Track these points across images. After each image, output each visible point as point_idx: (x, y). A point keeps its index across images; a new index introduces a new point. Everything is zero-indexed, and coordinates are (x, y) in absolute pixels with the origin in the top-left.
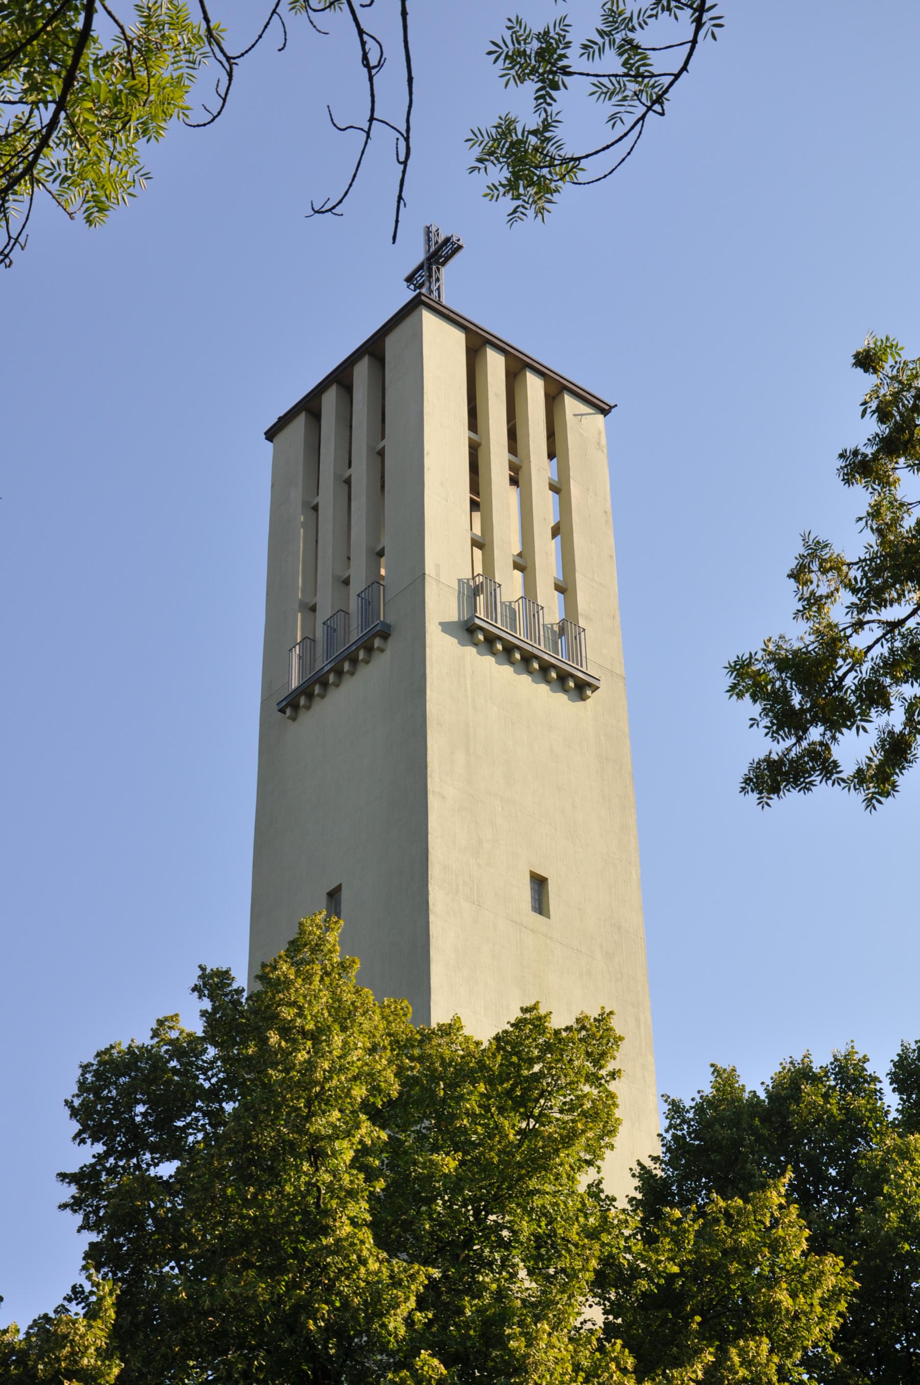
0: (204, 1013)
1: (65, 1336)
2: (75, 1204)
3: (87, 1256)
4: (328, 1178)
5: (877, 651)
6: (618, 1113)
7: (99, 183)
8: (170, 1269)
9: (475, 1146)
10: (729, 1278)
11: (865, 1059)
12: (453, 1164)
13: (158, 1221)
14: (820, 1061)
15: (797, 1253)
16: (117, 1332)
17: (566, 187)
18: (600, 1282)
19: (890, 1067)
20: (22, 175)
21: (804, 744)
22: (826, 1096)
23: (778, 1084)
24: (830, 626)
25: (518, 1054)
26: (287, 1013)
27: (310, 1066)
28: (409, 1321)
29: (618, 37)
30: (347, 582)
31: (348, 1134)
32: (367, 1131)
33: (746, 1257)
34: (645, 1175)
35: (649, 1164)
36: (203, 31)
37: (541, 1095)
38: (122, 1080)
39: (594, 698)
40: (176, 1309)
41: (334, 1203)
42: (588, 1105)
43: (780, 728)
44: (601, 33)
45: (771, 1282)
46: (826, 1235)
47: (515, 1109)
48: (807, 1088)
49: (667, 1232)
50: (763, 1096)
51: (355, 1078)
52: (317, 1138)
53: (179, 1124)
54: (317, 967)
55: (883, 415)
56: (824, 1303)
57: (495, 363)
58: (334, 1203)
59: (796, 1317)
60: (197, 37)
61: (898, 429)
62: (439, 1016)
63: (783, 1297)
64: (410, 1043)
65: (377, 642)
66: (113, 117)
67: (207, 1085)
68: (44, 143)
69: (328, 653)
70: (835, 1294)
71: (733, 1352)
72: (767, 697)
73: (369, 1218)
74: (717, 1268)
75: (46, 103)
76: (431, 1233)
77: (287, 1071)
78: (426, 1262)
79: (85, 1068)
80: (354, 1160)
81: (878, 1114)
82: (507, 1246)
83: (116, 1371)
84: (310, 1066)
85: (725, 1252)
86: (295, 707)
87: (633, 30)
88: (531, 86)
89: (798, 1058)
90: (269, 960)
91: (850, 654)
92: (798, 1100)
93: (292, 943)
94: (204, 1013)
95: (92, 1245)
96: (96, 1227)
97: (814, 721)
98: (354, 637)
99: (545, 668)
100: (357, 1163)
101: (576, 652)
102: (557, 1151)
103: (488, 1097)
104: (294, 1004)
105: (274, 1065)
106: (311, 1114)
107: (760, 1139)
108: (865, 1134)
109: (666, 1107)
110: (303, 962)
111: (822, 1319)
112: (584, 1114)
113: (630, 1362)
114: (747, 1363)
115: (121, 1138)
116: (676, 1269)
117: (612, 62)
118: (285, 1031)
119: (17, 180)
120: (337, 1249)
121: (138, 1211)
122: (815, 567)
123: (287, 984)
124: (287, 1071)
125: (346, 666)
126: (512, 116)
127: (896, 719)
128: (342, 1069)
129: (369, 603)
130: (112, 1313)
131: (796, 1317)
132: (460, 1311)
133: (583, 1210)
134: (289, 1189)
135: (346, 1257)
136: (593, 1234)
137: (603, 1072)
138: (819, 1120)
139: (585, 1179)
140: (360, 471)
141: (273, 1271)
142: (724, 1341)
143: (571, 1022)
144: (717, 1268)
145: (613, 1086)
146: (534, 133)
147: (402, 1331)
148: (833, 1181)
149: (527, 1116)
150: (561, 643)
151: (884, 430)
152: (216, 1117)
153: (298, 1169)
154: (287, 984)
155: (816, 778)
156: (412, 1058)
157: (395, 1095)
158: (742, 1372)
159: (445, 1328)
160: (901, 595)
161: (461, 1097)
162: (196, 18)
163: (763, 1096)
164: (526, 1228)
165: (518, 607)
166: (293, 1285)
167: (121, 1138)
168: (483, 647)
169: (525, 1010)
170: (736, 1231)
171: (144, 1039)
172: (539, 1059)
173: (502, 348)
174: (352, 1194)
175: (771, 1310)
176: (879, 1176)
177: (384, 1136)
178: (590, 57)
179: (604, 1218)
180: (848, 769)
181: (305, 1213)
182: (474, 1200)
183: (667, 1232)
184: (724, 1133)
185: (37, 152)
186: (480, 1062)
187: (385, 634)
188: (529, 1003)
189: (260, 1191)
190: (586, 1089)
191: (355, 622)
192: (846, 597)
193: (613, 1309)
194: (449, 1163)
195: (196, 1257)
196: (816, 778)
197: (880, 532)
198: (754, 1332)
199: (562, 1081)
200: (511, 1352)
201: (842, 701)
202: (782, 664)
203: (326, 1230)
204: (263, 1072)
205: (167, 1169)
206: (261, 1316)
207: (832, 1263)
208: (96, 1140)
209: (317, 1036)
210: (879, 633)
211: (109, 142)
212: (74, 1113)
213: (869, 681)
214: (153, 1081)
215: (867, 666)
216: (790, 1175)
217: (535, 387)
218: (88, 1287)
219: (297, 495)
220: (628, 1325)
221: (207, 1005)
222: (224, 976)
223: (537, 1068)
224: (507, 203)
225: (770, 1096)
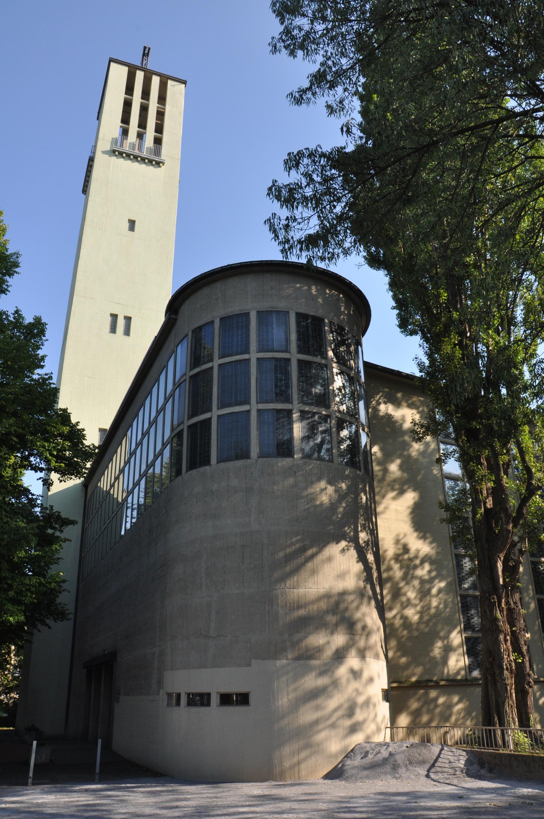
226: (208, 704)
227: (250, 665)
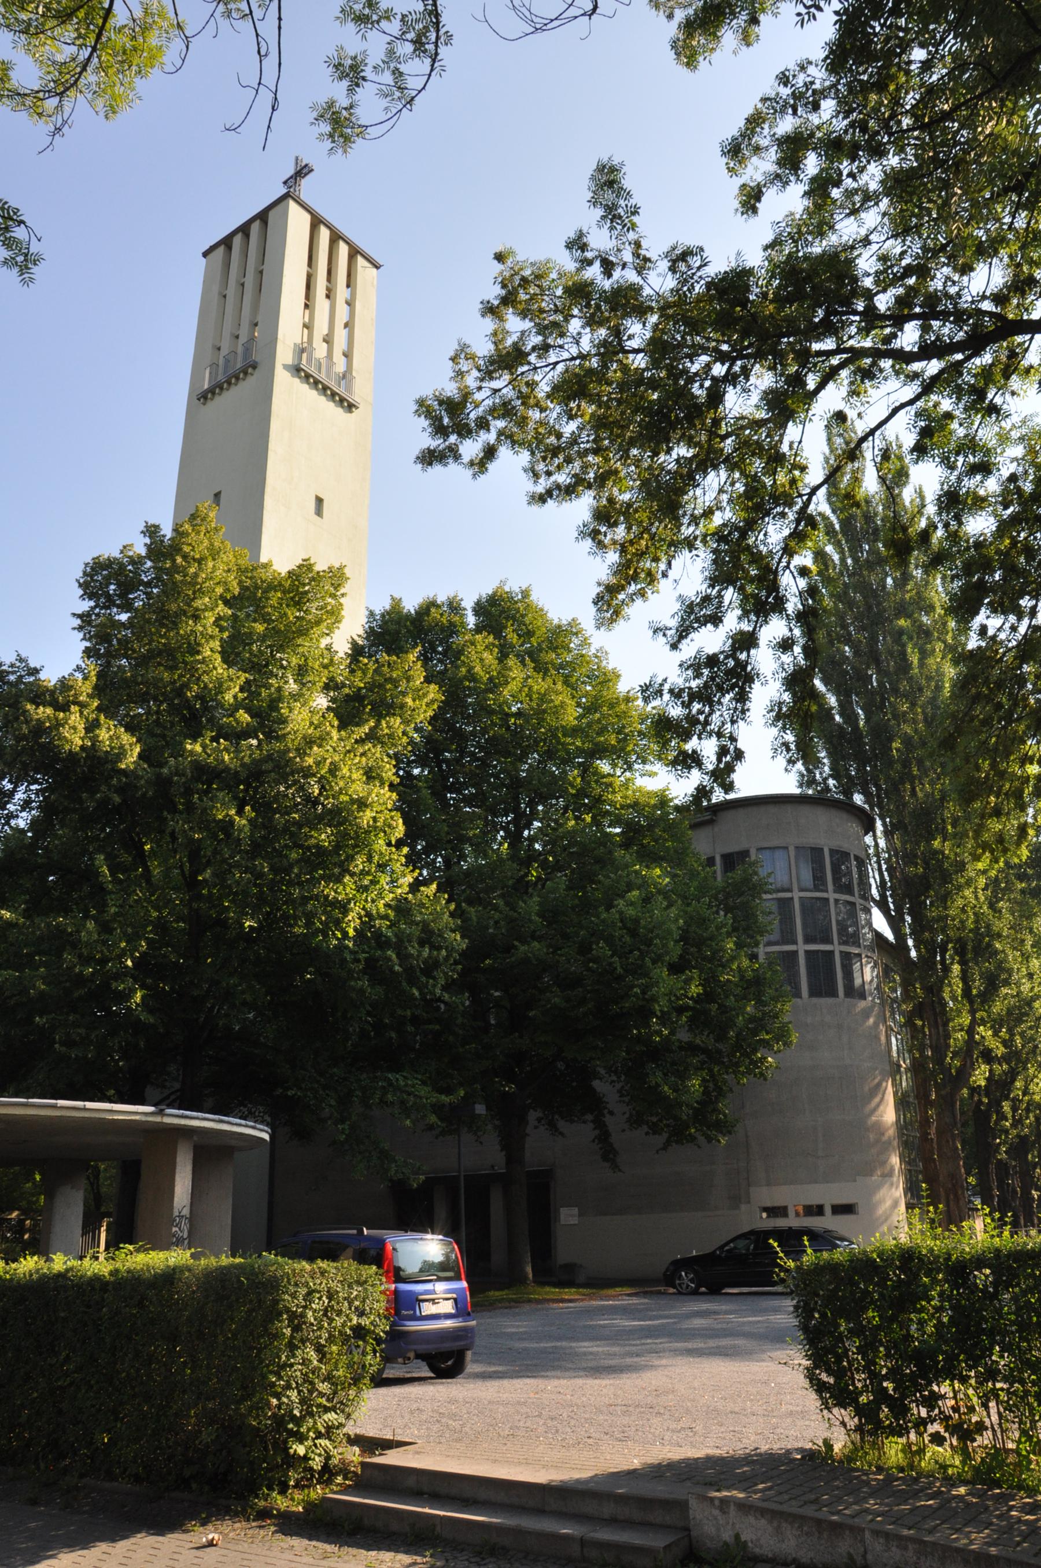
0: (146, 544)
1: (72, 686)
2: (80, 628)
3: (84, 652)
4: (201, 629)
5: (487, 402)
6: (343, 613)
7: (113, 97)
8: (124, 662)
9: (274, 621)
10: (386, 691)
11: (462, 600)
12: (262, 629)
13: (118, 640)
14: (441, 599)
15: (418, 682)
16: (96, 687)
17: (359, 141)
18: (327, 687)
19: (472, 604)
20: (72, 85)
21: (447, 443)
22: (442, 615)
23: (421, 607)
24: (466, 387)
25: (298, 581)
26: (186, 549)
27: (196, 575)
28: (235, 697)
29: (392, 65)
30: (237, 337)
31: (212, 609)
32: (222, 609)
33: (395, 682)
34: (354, 644)
35: (356, 638)
36: (175, 22)
37: (308, 601)
38: (105, 572)
39: (355, 412)
40: (125, 680)
41: (203, 641)
42: (329, 608)
43: (436, 434)
44: (384, 62)
45: (404, 694)
46: (432, 676)
47: (295, 606)
48: (433, 610)
49: (360, 669)
50: (413, 612)
51: (218, 583)
52: (197, 609)
53: (131, 596)
54: (203, 528)
55: (504, 286)
56: (427, 705)
57: (324, 234)
58: (203, 641)
59: (414, 710)
60: (172, 25)
61: (509, 293)
62: (263, 559)
63: (409, 701)
64: (246, 570)
65: (250, 370)
66: (122, 62)
67: (146, 580)
68: (84, 69)
69: (225, 373)
70: (433, 701)
71: (383, 722)
72: (432, 418)
73: (219, 649)
74: (381, 686)
75: (86, 46)
76: (249, 659)
77: (184, 576)
78: (245, 672)
79: (86, 565)
80: (214, 622)
81: (464, 625)
82: (285, 668)
83: (96, 704)
84: (196, 575)
85: (386, 680)
87: (400, 63)
88: (345, 83)
89: (431, 596)
90: (180, 522)
91: (474, 402)
92: (428, 615)
93: (192, 515)
94: (146, 544)
95: (86, 648)
96: (90, 640)
97: (453, 432)
98: (239, 366)
99: (334, 394)
100: (217, 623)
101: (349, 388)
102: (312, 628)
103: (282, 599)
104: (190, 544)
105: (178, 573)
106: (195, 598)
107: (409, 631)
108: (457, 633)
109: (367, 613)
110: (196, 525)
111: (425, 711)
112: (327, 612)
113: (336, 723)
114: (389, 727)
115: (102, 600)
116: (362, 685)
117: (387, 78)
118: (185, 557)
119: (67, 89)
120: (203, 661)
121: (109, 634)
122: (462, 356)
123: (188, 534)
124: (184, 576)
125: (233, 381)
126: (335, 98)
127: (491, 437)
128: (211, 578)
129: (247, 350)
130: (94, 679)
131: (414, 710)
132: (260, 694)
133: (322, 656)
134: (182, 632)
135: (207, 665)
136: (325, 667)
137: (338, 593)
138: (437, 625)
139: (324, 642)
140: (250, 280)
141: (172, 669)
142: (379, 717)
143: (326, 568)
144: (381, 686)
145: (342, 600)
146: (345, 109)
147: (232, 701)
148: (440, 653)
149: (299, 610)
150: (343, 383)
151: (503, 292)
152: (149, 596)
153: (187, 624)
154: (188, 534)
155: (450, 460)
156: (247, 577)
157: (236, 593)
158: (386, 731)
159: (252, 701)
160: (501, 376)
161: (268, 599)
162: (172, 15)
163: (413, 612)
164: (294, 661)
165: (324, 362)
166: (181, 676)
167: (102, 600)
168: (304, 380)
169: (304, 560)
170: (392, 671)
171: (116, 554)
172: (309, 584)
173: (347, 242)
174: (212, 637)
175: (403, 706)
176: (460, 652)
177: (230, 612)
178: (377, 73)
179: (332, 660)
180: (466, 459)
181: (189, 644)
182: (270, 646)
183: (360, 669)
184: (393, 627)
185: (80, 73)
186: (280, 583)
188: (307, 557)
189: (168, 631)
190: (330, 600)
191: (240, 359)
192: (475, 373)
193: (333, 700)
194: (260, 628)
195: (135, 659)
196: (450, 460)
197: (495, 343)
198: (394, 714)
199: (318, 596)
200: (281, 715)
201: (467, 425)
202: (441, 403)
203: (198, 653)
204: (172, 576)
205: (124, 617)
206: (165, 687)
207: (433, 687)
208: (90, 599)
209: (199, 561)
210: (489, 393)
211: (121, 76)
212: (80, 585)
213: (482, 417)
214: (119, 575)
215: (481, 409)
216: (419, 648)
217: (343, 249)
218: (83, 666)
219: (216, 288)
220: (338, 707)
221: (148, 541)
222: (157, 527)
223: (307, 588)
224: (328, 144)
225: (416, 612)
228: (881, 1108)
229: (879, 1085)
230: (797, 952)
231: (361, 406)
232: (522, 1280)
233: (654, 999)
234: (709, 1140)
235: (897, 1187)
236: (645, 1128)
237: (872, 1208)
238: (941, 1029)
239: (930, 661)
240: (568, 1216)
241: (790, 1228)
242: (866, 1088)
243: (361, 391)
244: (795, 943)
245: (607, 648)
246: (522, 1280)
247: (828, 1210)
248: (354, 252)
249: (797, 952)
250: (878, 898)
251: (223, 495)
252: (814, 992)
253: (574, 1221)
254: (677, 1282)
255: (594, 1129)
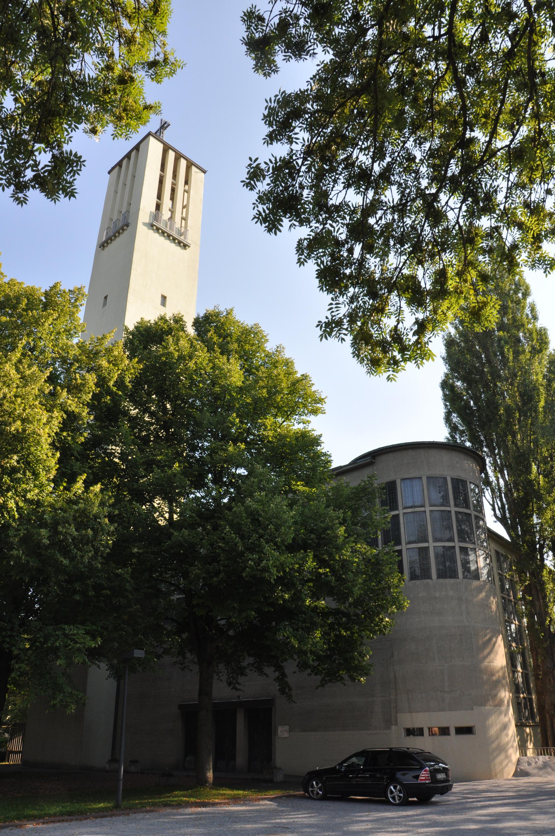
39: (188, 250)
57: (171, 155)
65: (125, 228)
86: (104, 247)
125: (117, 234)
140: (128, 183)
173: (186, 159)
187: (127, 225)
217: (183, 163)
219: (113, 189)
226: (448, 734)
227: (472, 709)
228: (492, 656)
229: (490, 640)
230: (428, 547)
231: (191, 246)
232: (202, 782)
233: (266, 569)
234: (353, 679)
235: (506, 714)
236: (309, 671)
237: (485, 729)
238: (541, 601)
239: (521, 357)
240: (282, 732)
241: (391, 749)
242: (481, 642)
243: (192, 238)
244: (427, 541)
245: (284, 345)
246: (202, 782)
247: (452, 731)
248: (190, 164)
249: (428, 547)
250: (500, 516)
251: (108, 298)
252: (442, 575)
253: (286, 735)
254: (310, 789)
255: (274, 671)
